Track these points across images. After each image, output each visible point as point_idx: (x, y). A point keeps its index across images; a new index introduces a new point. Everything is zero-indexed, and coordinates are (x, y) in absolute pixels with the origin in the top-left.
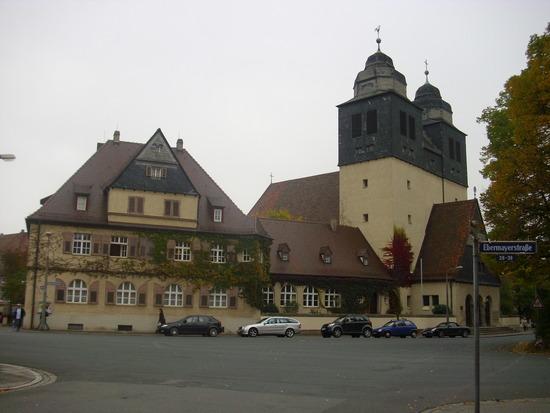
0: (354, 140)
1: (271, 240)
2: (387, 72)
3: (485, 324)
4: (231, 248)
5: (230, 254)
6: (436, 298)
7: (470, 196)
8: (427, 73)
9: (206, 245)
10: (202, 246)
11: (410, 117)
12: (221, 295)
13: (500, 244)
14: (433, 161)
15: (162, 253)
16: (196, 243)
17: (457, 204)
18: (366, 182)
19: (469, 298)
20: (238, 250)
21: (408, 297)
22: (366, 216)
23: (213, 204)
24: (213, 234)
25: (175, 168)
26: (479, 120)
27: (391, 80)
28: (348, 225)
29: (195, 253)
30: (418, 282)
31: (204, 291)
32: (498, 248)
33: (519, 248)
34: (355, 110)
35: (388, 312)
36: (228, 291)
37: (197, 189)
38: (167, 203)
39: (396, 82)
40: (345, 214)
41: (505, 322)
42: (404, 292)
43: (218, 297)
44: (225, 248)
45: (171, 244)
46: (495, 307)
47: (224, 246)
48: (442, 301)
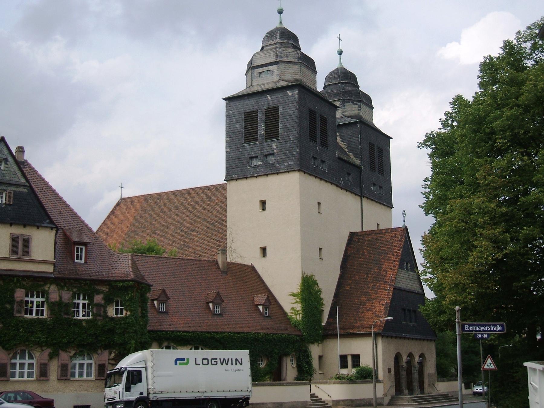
0: (248, 146)
1: (149, 286)
2: (291, 54)
3: (418, 391)
4: (98, 299)
5: (98, 305)
6: (356, 358)
7: (397, 222)
8: (340, 53)
9: (66, 296)
10: (61, 297)
11: (321, 116)
12: (86, 362)
13: (478, 325)
14: (349, 174)
15: (8, 306)
16: (54, 293)
17: (378, 233)
18: (263, 203)
19: (398, 357)
20: (109, 300)
21: (320, 357)
22: (264, 250)
23: (74, 237)
24: (76, 280)
25: (24, 190)
26: (421, 145)
27: (297, 68)
28: (239, 261)
29: (53, 306)
30: (334, 336)
31: (64, 356)
32: (476, 328)
33: (491, 328)
34: (250, 105)
35: (297, 379)
36: (95, 356)
37: (54, 219)
38: (14, 239)
39: (305, 69)
40: (233, 246)
41: (443, 387)
42: (315, 350)
43: (81, 366)
44: (91, 299)
45: (19, 294)
46: (430, 368)
47: (89, 297)
48: (366, 361)
